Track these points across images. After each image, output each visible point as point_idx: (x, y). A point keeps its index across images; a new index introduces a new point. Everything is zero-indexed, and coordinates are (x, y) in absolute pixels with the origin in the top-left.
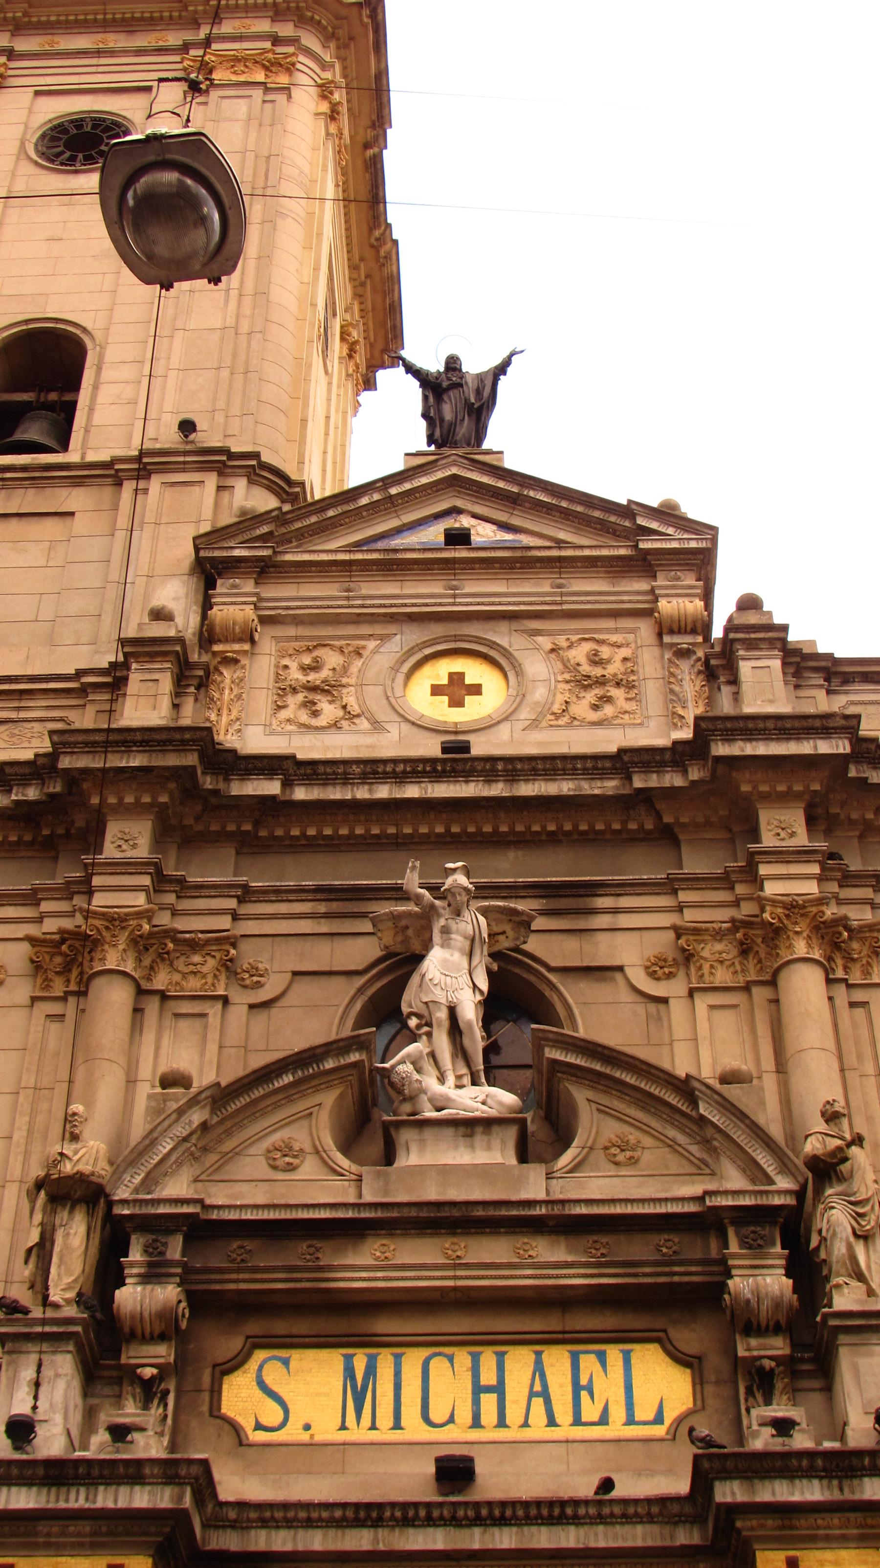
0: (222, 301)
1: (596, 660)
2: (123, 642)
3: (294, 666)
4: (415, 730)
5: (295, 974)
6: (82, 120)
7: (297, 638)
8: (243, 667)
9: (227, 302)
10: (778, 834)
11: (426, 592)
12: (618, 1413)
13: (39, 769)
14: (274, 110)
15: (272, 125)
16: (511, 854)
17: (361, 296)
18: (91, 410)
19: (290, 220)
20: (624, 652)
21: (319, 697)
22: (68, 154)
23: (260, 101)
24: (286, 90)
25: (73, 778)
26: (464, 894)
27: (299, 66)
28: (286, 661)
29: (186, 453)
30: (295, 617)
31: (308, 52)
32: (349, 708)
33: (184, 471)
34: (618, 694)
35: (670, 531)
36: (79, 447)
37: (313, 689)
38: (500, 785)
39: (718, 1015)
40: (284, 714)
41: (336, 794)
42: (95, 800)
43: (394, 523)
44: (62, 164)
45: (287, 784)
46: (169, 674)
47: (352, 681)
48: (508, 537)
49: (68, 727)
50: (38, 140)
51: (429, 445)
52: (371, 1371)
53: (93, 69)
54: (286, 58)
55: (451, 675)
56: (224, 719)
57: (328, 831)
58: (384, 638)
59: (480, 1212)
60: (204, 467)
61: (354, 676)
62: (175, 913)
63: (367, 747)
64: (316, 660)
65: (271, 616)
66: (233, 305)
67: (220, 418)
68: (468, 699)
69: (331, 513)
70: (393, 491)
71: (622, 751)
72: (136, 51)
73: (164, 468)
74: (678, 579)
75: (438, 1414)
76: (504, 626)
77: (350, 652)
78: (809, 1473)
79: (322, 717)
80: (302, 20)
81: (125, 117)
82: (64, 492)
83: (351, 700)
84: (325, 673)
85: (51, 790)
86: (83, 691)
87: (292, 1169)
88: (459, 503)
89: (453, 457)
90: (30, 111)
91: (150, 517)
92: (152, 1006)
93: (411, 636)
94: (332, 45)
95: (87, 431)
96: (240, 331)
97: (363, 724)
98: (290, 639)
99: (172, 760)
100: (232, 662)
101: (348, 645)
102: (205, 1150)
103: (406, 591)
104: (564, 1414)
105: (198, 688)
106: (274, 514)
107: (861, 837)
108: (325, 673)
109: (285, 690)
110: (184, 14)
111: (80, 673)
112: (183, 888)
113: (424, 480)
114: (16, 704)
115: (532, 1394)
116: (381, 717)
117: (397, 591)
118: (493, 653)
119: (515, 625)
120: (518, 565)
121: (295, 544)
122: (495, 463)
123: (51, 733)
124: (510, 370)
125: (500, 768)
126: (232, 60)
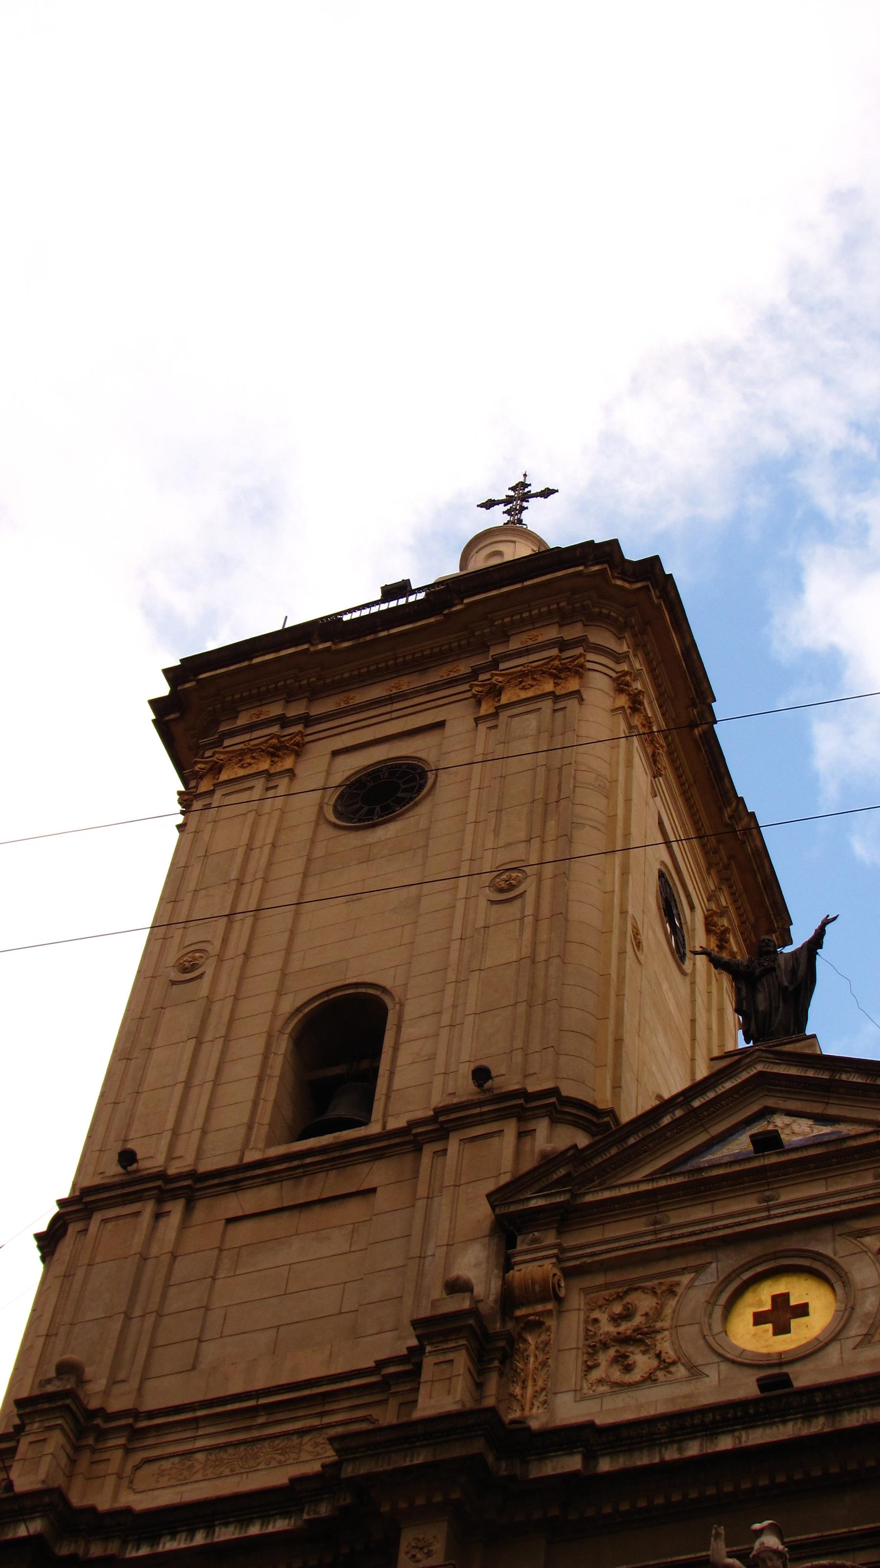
0: (517, 930)
2: (416, 1324)
3: (603, 1317)
4: (735, 1369)
6: (379, 770)
7: (606, 1286)
8: (548, 1329)
9: (522, 930)
10: (414, 1556)
11: (739, 1209)
13: (323, 1483)
14: (565, 717)
15: (563, 734)
17: (728, 879)
18: (392, 1073)
19: (588, 829)
21: (631, 1349)
22: (366, 808)
23: (549, 711)
24: (577, 694)
26: (775, 1557)
27: (589, 665)
28: (596, 1314)
29: (481, 1104)
30: (601, 1262)
31: (599, 649)
32: (663, 1355)
33: (482, 1122)
36: (380, 1117)
37: (624, 1340)
38: (821, 1420)
40: (595, 1374)
42: (385, 1508)
43: (703, 1138)
44: (360, 821)
45: (590, 1457)
46: (464, 1352)
47: (666, 1324)
48: (826, 1130)
49: (371, 1427)
50: (336, 801)
51: (748, 1042)
53: (387, 717)
54: (573, 661)
55: (775, 1298)
56: (530, 1391)
57: (642, 1503)
58: (698, 1270)
60: (501, 1115)
61: (669, 1318)
63: (684, 1397)
64: (626, 1308)
65: (575, 1266)
66: (528, 934)
67: (518, 1058)
68: (794, 1323)
69: (632, 1141)
70: (696, 1103)
72: (427, 689)
76: (826, 1233)
77: (663, 1292)
79: (636, 1371)
80: (591, 619)
81: (420, 759)
82: (364, 1168)
83: (665, 1346)
84: (638, 1320)
85: (342, 1502)
86: (386, 1383)
88: (770, 1102)
89: (757, 1053)
90: (328, 773)
91: (449, 1180)
93: (718, 1267)
95: (388, 1097)
96: (537, 959)
97: (680, 1371)
99: (457, 1451)
100: (536, 1325)
101: (661, 1284)
103: (718, 1212)
105: (503, 1362)
106: (569, 1154)
108: (638, 1320)
109: (594, 1346)
110: (472, 640)
111: (381, 1364)
113: (728, 1085)
114: (319, 1410)
116: (699, 1360)
117: (708, 1214)
118: (817, 1265)
120: (835, 1160)
121: (597, 1182)
122: (807, 1051)
123: (332, 1440)
124: (826, 940)
125: (818, 1400)
126: (520, 676)
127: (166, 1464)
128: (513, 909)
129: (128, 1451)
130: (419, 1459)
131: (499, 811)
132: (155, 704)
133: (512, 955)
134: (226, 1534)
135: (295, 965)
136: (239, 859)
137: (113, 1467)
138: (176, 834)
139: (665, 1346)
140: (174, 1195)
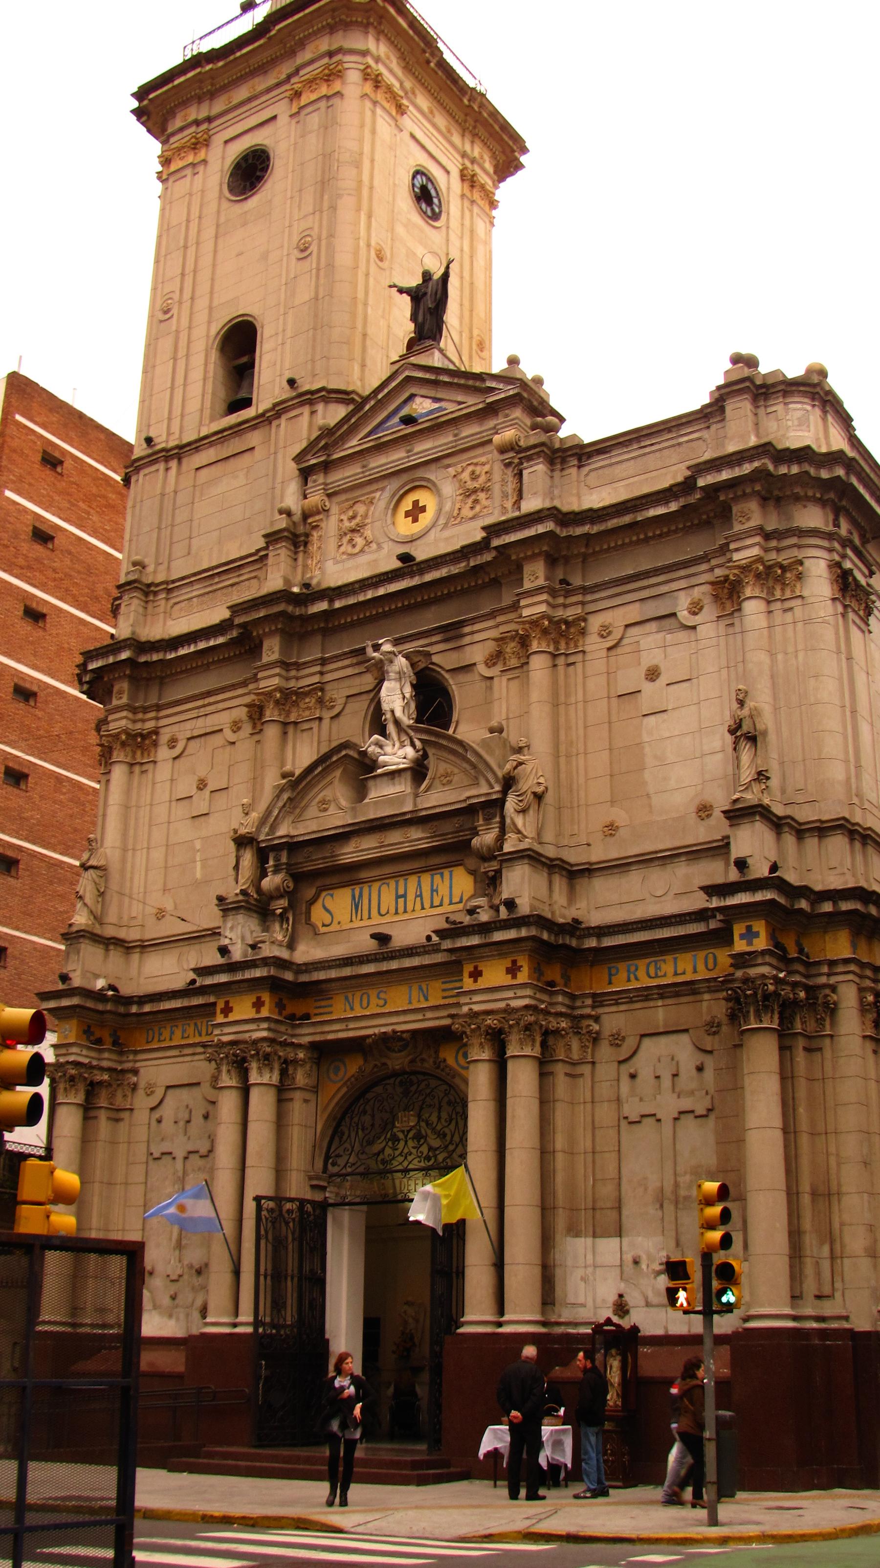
1: (474, 477)
5: (348, 697)
7: (347, 500)
11: (396, 457)
12: (446, 901)
16: (433, 608)
20: (487, 468)
25: (244, 626)
27: (346, 66)
34: (482, 496)
35: (501, 386)
37: (353, 531)
39: (512, 683)
40: (342, 549)
41: (351, 601)
48: (437, 405)
52: (361, 895)
58: (383, 489)
59: (387, 821)
60: (302, 404)
62: (297, 679)
69: (353, 420)
70: (380, 396)
71: (463, 548)
73: (286, 410)
74: (507, 416)
75: (383, 912)
78: (473, 933)
87: (332, 809)
92: (291, 730)
93: (393, 485)
94: (371, 30)
97: (374, 546)
98: (343, 502)
102: (295, 808)
104: (427, 905)
107: (583, 562)
112: (298, 666)
113: (394, 384)
115: (416, 896)
119: (439, 464)
127: (183, 604)
128: (306, 264)
129: (167, 599)
130: (261, 615)
131: (300, 190)
132: (134, 112)
133: (307, 298)
134: (202, 645)
135: (216, 303)
136: (183, 229)
137: (161, 609)
138: (159, 201)
139: (368, 532)
140: (171, 457)
